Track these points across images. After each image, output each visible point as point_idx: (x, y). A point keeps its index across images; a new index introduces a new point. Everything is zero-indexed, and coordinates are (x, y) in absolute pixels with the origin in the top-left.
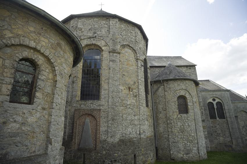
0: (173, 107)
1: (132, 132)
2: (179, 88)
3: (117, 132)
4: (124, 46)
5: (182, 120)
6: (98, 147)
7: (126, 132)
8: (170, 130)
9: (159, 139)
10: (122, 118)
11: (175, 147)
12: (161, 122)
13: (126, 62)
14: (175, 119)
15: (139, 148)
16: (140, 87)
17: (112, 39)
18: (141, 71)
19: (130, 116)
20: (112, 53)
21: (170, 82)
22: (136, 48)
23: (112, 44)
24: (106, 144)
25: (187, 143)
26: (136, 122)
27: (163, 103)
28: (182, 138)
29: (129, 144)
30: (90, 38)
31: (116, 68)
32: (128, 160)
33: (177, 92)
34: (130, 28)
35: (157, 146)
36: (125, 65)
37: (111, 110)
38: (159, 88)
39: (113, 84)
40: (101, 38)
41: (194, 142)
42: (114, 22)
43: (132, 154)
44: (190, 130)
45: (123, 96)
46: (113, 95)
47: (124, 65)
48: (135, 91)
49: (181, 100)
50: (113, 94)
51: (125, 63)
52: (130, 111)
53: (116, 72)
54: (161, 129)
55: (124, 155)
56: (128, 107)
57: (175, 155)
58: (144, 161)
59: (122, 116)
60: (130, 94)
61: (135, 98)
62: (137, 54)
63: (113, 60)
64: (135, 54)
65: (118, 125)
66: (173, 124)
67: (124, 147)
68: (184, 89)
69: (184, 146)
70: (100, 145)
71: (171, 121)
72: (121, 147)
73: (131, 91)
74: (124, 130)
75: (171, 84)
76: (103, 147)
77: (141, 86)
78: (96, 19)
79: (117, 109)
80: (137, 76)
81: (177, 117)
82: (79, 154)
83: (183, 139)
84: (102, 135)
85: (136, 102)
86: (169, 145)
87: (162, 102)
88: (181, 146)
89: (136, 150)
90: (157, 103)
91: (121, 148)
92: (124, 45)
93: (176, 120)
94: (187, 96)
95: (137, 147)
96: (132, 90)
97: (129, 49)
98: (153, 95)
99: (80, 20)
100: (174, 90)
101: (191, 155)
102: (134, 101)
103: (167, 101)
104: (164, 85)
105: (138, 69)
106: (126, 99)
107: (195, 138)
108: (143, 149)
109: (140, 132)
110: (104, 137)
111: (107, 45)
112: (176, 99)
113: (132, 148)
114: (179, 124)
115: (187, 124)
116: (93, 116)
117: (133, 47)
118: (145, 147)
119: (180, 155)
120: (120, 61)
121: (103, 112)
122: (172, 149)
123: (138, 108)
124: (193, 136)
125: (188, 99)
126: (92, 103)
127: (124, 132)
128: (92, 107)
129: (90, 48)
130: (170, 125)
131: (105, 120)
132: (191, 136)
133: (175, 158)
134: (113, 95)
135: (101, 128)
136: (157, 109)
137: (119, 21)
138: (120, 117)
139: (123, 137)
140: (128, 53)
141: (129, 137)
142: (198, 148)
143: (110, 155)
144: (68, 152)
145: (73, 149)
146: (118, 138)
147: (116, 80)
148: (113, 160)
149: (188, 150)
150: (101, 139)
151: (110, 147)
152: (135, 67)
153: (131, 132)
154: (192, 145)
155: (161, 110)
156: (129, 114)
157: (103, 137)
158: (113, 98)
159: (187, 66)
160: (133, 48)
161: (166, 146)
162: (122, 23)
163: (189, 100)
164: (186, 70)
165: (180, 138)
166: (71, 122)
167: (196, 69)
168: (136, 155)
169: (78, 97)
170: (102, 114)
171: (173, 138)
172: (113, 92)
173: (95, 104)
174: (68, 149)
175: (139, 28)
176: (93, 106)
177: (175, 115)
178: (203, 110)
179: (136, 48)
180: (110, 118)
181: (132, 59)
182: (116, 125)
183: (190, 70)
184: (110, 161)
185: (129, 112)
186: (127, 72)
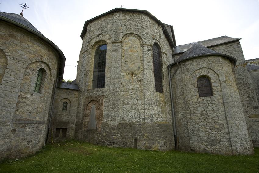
0: (192, 90)
1: (134, 116)
2: (199, 67)
3: (117, 115)
5: (204, 104)
7: (127, 116)
8: (188, 116)
9: (178, 126)
10: (123, 103)
11: (195, 136)
12: (179, 108)
13: (129, 49)
14: (194, 104)
15: (141, 132)
17: (114, 31)
19: (132, 100)
20: (114, 44)
21: (187, 63)
22: (142, 34)
23: (115, 36)
25: (212, 131)
26: (140, 107)
27: (181, 87)
28: (204, 126)
29: (129, 128)
30: (98, 36)
31: (118, 57)
32: (127, 143)
33: (196, 72)
34: (136, 16)
35: (175, 134)
36: (128, 52)
38: (176, 71)
39: (114, 71)
41: (222, 131)
43: (132, 138)
44: (216, 116)
45: (125, 82)
48: (139, 76)
49: (204, 82)
50: (114, 80)
51: (129, 51)
52: (132, 95)
54: (180, 116)
55: (123, 138)
56: (130, 91)
57: (195, 145)
58: (147, 146)
60: (133, 79)
61: (140, 83)
63: (116, 50)
64: (141, 40)
66: (192, 109)
67: (123, 131)
68: (205, 67)
69: (207, 135)
71: (189, 106)
72: (120, 130)
75: (188, 65)
76: (104, 129)
78: (103, 19)
79: (117, 94)
80: (142, 61)
81: (197, 101)
82: (87, 134)
83: (205, 127)
84: (104, 118)
85: (141, 86)
86: (189, 133)
87: (180, 86)
88: (203, 135)
89: (137, 134)
90: (175, 88)
91: (120, 131)
92: (127, 34)
93: (196, 104)
94: (211, 75)
95: (138, 131)
96: (136, 75)
97: (133, 37)
98: (171, 80)
99: (92, 24)
100: (192, 71)
101: (218, 147)
102: (138, 86)
103: (185, 84)
104: (181, 68)
105: (143, 54)
106: (128, 84)
107: (224, 126)
108: (146, 134)
111: (110, 38)
112: (195, 80)
113: (132, 132)
114: (200, 109)
115: (210, 109)
116: (98, 102)
118: (149, 133)
119: (203, 146)
120: (123, 49)
122: (191, 138)
123: (143, 92)
124: (220, 124)
125: (212, 78)
126: (98, 91)
128: (98, 94)
130: (188, 110)
131: (107, 105)
132: (218, 124)
133: (196, 149)
136: (175, 94)
137: (122, 13)
139: (124, 120)
140: (133, 41)
141: (130, 121)
142: (230, 139)
143: (110, 137)
147: (117, 67)
148: (112, 141)
149: (213, 140)
151: (110, 129)
152: (140, 53)
153: (133, 117)
154: (219, 135)
155: (179, 94)
156: (131, 99)
157: (105, 120)
158: (114, 84)
159: (226, 44)
160: (137, 35)
161: (185, 135)
163: (214, 80)
164: (225, 48)
165: (202, 126)
167: (240, 45)
168: (137, 139)
169: (90, 87)
171: (192, 126)
172: (114, 79)
173: (100, 92)
175: (146, 13)
176: (99, 93)
177: (194, 99)
178: (254, 94)
179: (141, 35)
181: (136, 45)
183: (232, 47)
184: (109, 142)
186: (130, 59)
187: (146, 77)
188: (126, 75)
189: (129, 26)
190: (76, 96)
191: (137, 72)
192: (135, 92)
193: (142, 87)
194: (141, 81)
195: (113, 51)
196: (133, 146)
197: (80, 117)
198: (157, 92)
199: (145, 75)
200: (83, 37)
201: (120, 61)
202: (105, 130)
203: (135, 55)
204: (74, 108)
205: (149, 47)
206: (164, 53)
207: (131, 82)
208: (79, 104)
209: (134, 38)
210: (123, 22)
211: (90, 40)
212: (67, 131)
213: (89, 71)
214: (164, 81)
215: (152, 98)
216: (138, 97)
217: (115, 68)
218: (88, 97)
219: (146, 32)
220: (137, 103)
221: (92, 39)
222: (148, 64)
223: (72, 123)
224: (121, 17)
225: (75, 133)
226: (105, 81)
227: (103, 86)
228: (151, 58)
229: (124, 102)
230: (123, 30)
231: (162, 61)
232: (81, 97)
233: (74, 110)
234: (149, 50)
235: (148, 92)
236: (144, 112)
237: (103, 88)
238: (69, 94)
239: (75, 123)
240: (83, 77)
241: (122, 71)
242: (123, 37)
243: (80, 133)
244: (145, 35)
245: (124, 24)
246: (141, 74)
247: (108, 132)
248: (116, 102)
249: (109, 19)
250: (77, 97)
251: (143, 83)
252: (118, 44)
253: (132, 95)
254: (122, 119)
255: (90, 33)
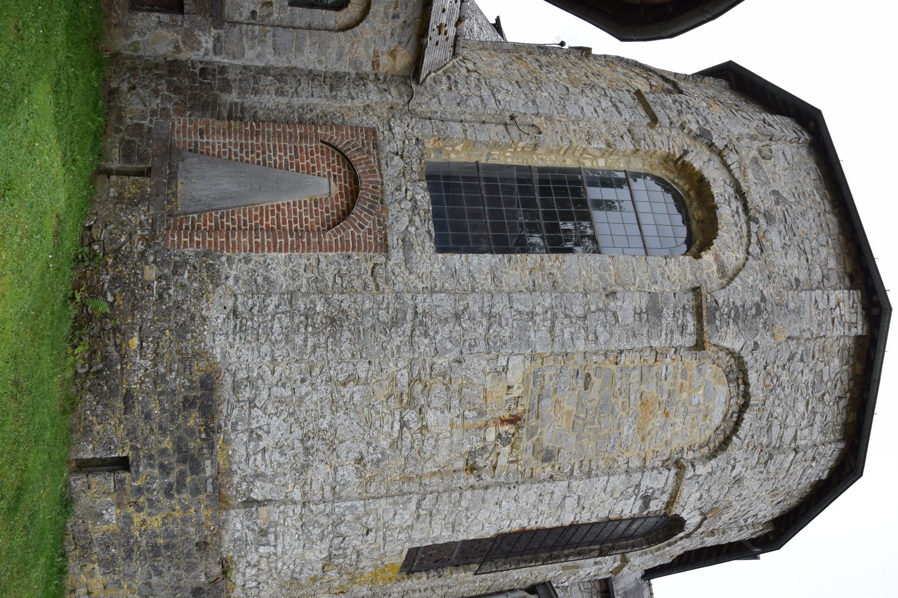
1: (262, 444)
4: (738, 373)
6: (179, 238)
7: (264, 409)
10: (342, 377)
13: (660, 389)
16: (528, 495)
17: (763, 299)
18: (617, 495)
22: (739, 455)
23: (739, 303)
24: (195, 285)
26: (319, 473)
30: (740, 194)
34: (832, 413)
36: (643, 388)
37: (387, 308)
40: (754, 245)
42: (845, 309)
46: (472, 319)
47: (638, 379)
51: (650, 389)
52: (386, 428)
53: (600, 329)
59: (352, 378)
61: (460, 464)
62: (710, 459)
64: (705, 450)
65: (302, 353)
70: (189, 251)
73: (499, 436)
74: (277, 391)
77: (533, 498)
79: (397, 341)
80: (586, 469)
84: (247, 261)
106: (455, 402)
109: (259, 503)
110: (233, 273)
116: (346, 213)
117: (741, 433)
120: (658, 354)
121: (375, 264)
123: (405, 488)
127: (265, 394)
129: (687, 202)
131: (329, 277)
134: (472, 319)
135: (283, 254)
137: (857, 338)
138: (351, 367)
139: (236, 388)
141: (234, 425)
144: (159, 101)
145: (173, 125)
146: (232, 351)
150: (224, 259)
153: (258, 444)
157: (234, 271)
160: (735, 431)
162: (851, 362)
166: (308, 116)
168: (126, 475)
169: (440, 151)
170: (362, 261)
173: (411, 222)
174: (176, 104)
175: (847, 468)
179: (736, 450)
180: (345, 305)
182: (306, 340)
185: (377, 424)
187: (493, 495)
188: (509, 388)
189: (784, 378)
190: (385, 60)
191: (526, 443)
192: (407, 442)
193: (435, 480)
194: (472, 468)
195: (653, 296)
196: (88, 452)
197: (256, 92)
198: (405, 553)
199: (505, 490)
200: (727, 79)
201: (592, 347)
202: (175, 273)
203: (625, 431)
204: (307, 49)
205: (665, 498)
206: (625, 561)
207: (464, 417)
208: (335, 81)
209: (717, 418)
210: (810, 345)
211: (719, 144)
212: (165, 17)
213: (536, 146)
214: (470, 574)
215: (372, 534)
216: (379, 460)
217: (555, 316)
218: (376, 146)
219: (749, 474)
220: (343, 456)
221: (720, 154)
222: (570, 502)
223: (217, 39)
224: (839, 331)
225: (157, 66)
226: (474, 258)
227: (443, 245)
228: (603, 514)
229: (344, 384)
230: (763, 350)
231: (581, 555)
232: (375, 97)
233: (299, 49)
234: (647, 500)
235: (406, 516)
236: (288, 501)
237: (430, 245)
238: (396, 16)
239: (217, 59)
240: (498, 102)
241: (533, 359)
242: (731, 353)
243: (156, 103)
244: (734, 473)
245: (801, 348)
246: (513, 467)
247: (161, 296)
248: (347, 334)
249: (827, 256)
250: (375, 64)
251: (462, 483)
252: (691, 328)
253: (386, 428)
254: (242, 375)
255: (753, 138)
